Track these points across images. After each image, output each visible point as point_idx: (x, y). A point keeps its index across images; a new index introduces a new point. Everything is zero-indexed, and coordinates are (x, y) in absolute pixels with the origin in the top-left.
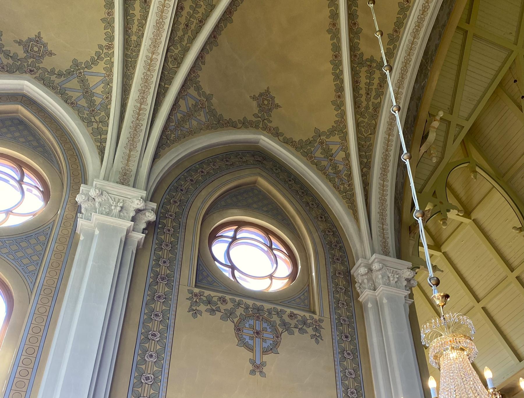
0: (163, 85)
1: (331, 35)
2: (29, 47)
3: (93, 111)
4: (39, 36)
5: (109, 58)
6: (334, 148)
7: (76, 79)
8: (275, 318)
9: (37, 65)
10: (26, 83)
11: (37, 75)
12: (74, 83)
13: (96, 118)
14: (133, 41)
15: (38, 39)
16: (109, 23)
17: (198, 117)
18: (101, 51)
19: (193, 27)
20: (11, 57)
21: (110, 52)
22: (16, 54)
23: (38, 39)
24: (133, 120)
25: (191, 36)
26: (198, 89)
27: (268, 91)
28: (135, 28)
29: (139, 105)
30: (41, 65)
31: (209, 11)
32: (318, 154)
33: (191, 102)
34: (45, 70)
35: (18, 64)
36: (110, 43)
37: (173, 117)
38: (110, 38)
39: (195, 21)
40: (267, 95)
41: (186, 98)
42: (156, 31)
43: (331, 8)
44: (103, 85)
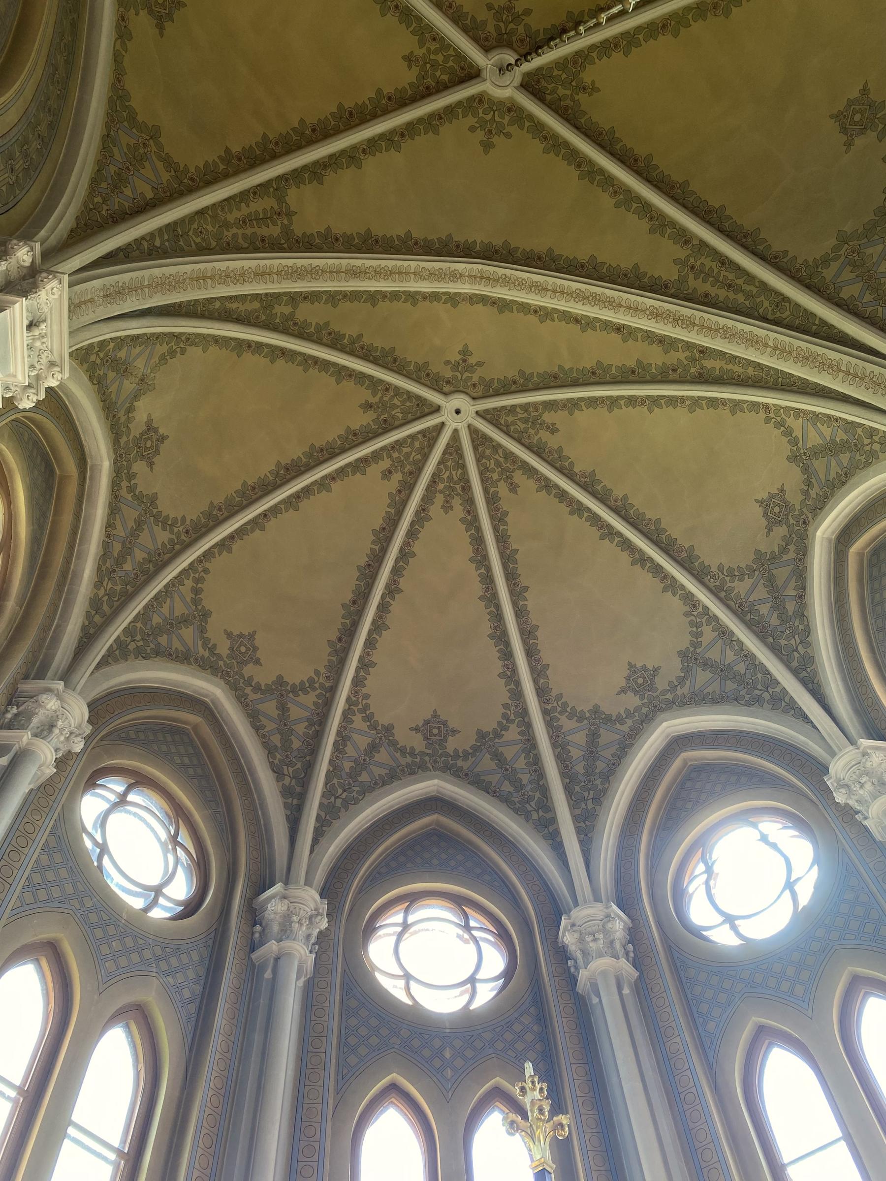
0: (816, 327)
1: (732, 7)
2: (774, 518)
3: (855, 445)
4: (761, 502)
5: (782, 411)
7: (814, 461)
9: (797, 512)
10: (819, 533)
11: (810, 515)
12: (819, 465)
13: (865, 443)
14: (755, 373)
15: (765, 505)
16: (736, 406)
17: (874, 260)
18: (773, 420)
19: (731, 276)
20: (786, 546)
21: (774, 409)
22: (783, 538)
23: (765, 505)
24: (863, 387)
25: (744, 279)
26: (826, 261)
27: (836, 117)
28: (738, 369)
29: (841, 374)
30: (798, 507)
31: (708, 249)
33: (847, 275)
34: (803, 503)
35: (796, 538)
36: (761, 406)
37: (869, 310)
38: (755, 406)
39: (724, 273)
40: (845, 116)
41: (840, 284)
42: (736, 340)
43: (691, 20)
44: (818, 423)
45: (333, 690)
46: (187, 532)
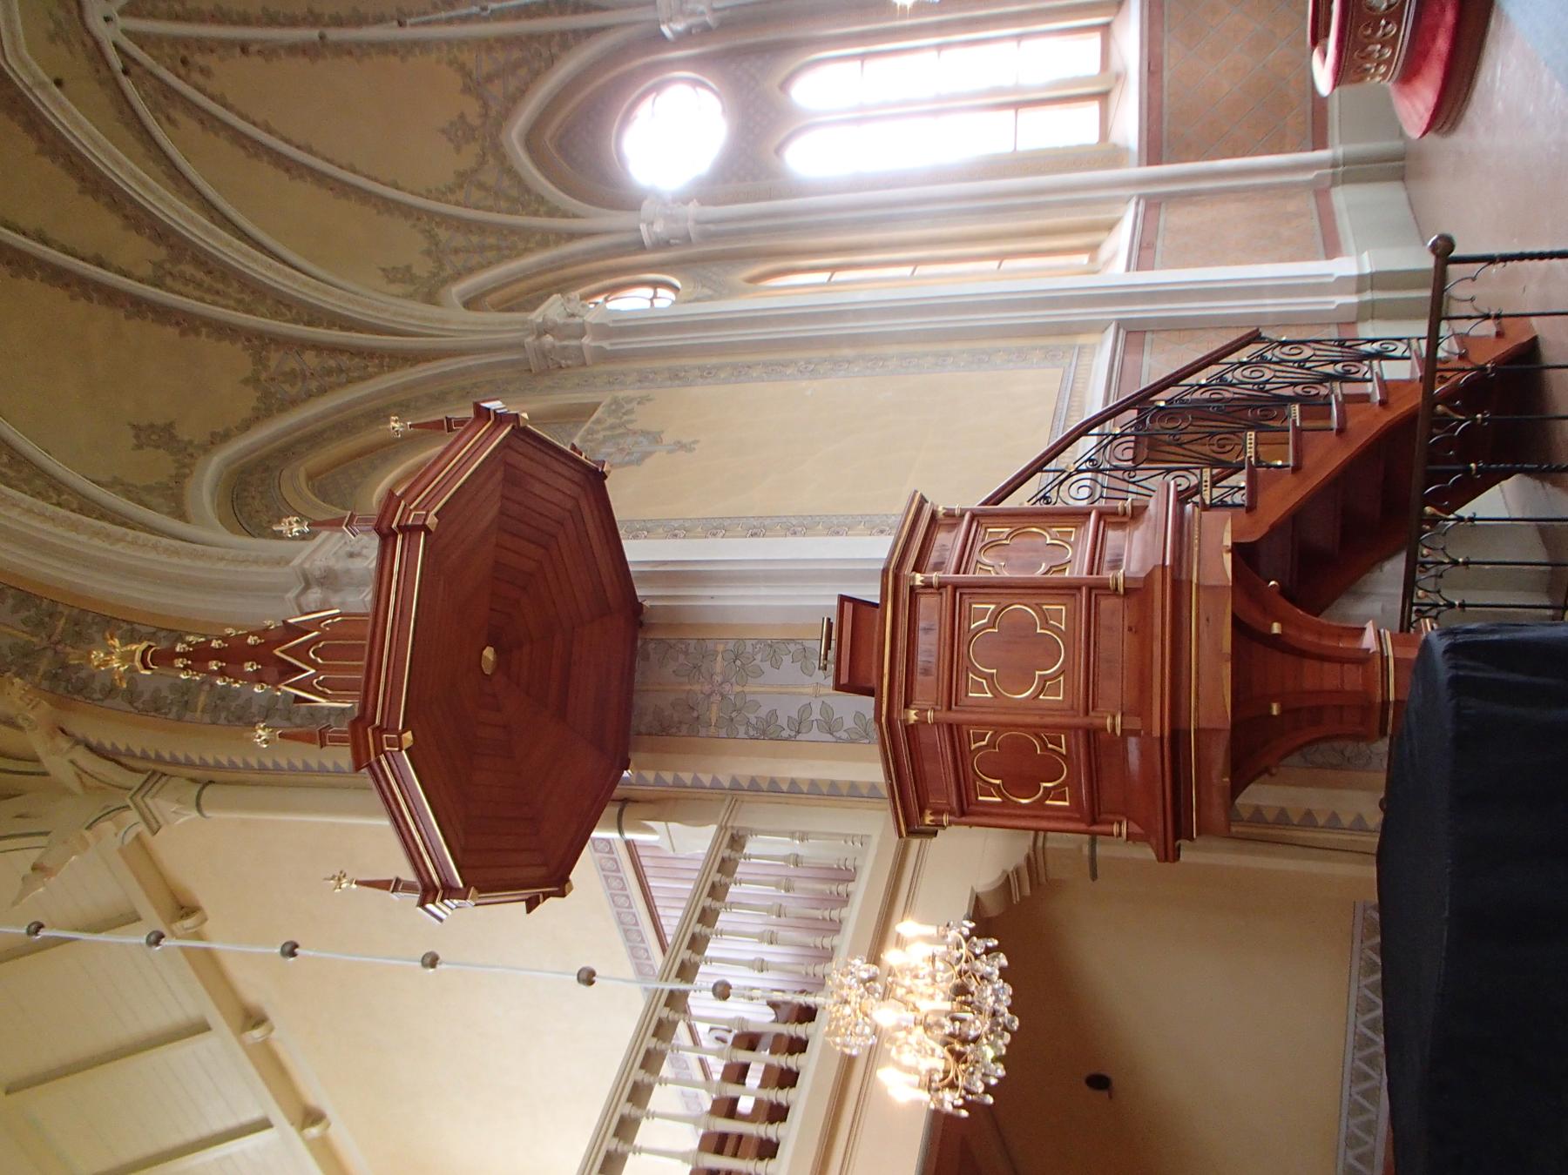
6: (292, 363)
8: (600, 436)
32: (292, 390)
45: (449, 42)
46: (419, 219)
